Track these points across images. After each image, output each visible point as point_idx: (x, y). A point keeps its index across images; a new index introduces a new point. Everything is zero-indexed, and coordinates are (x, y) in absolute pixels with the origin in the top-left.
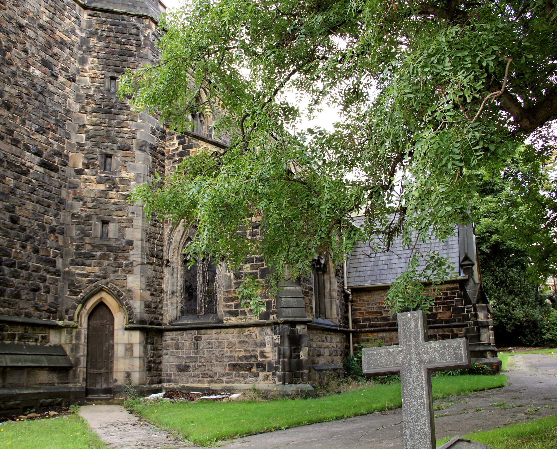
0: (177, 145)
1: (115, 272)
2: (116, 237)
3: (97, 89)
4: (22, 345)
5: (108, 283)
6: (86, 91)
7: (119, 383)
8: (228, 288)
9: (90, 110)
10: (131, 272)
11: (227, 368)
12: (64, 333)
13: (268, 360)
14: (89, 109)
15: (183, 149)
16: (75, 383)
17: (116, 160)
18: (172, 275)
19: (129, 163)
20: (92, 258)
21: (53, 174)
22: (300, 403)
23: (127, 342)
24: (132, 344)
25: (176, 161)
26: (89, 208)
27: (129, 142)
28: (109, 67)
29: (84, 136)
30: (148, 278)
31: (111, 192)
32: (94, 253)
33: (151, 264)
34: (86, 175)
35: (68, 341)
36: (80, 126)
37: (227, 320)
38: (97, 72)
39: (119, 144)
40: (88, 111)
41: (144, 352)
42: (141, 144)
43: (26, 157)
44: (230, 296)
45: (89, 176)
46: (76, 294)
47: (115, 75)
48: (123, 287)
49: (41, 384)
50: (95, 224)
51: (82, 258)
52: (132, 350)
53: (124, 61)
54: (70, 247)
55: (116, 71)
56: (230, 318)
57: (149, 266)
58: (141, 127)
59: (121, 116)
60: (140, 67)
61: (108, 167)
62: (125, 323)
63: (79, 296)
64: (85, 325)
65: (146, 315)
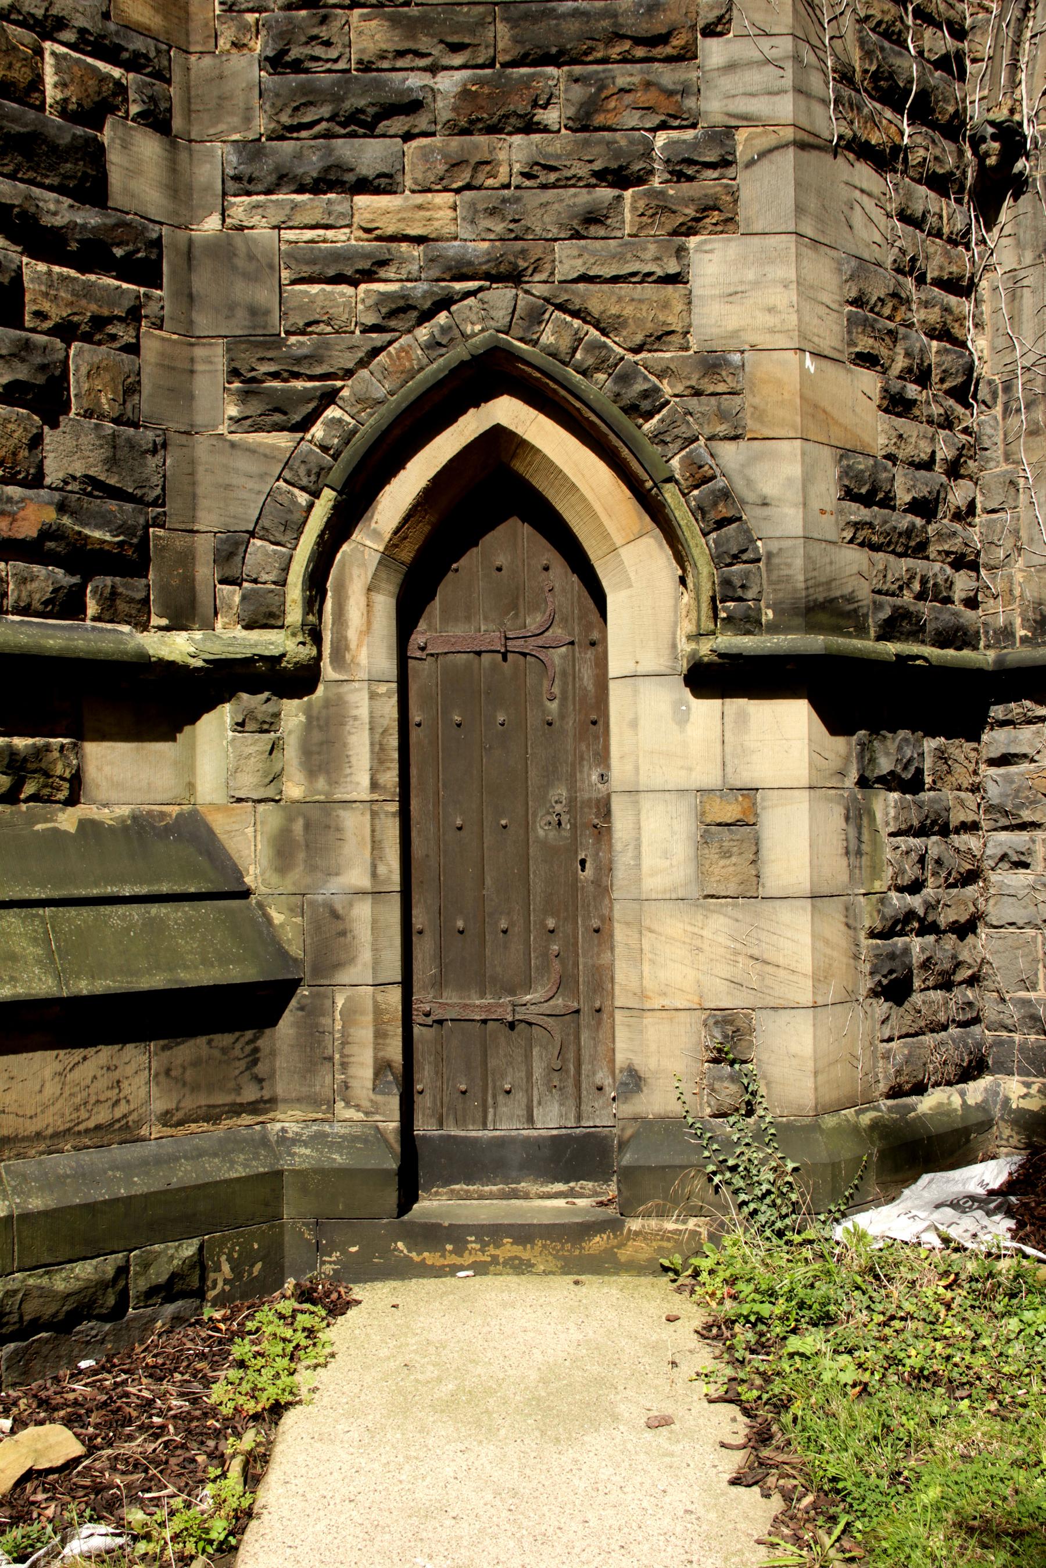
5: (535, 317)
7: (658, 1101)
10: (717, 215)
12: (215, 730)
20: (398, 124)
23: (708, 776)
30: (863, 267)
32: (415, 81)
33: (884, 159)
35: (248, 783)
41: (853, 852)
48: (659, 338)
57: (864, 174)
62: (688, 627)
65: (854, 558)
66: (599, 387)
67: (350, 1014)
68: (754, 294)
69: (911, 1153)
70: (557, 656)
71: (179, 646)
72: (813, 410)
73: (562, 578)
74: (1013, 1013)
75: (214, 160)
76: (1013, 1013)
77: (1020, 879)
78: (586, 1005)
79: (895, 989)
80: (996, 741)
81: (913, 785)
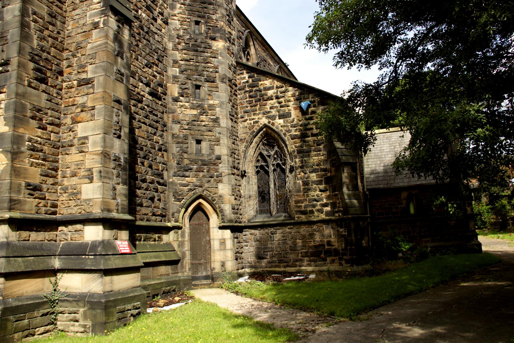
0: (247, 78)
1: (209, 181)
2: (208, 153)
3: (185, 31)
4: (146, 245)
5: (203, 191)
6: (177, 32)
7: (216, 271)
8: (298, 192)
9: (181, 48)
10: (221, 181)
11: (300, 255)
12: (172, 233)
13: (334, 247)
14: (180, 47)
15: (253, 81)
16: (183, 272)
17: (204, 90)
18: (249, 183)
19: (214, 92)
20: (190, 171)
21: (157, 101)
22: (366, 280)
23: (221, 238)
24: (225, 239)
25: (247, 91)
26: (185, 129)
27: (213, 75)
28: (194, 12)
29: (178, 70)
30: (233, 186)
31: (201, 116)
32: (192, 166)
33: (233, 174)
34: (181, 102)
35: (175, 239)
36: (174, 61)
37: (298, 218)
38: (184, 16)
39: (205, 77)
40: (179, 49)
41: (233, 245)
42: (222, 77)
43: (140, 87)
44: (300, 199)
45: (184, 103)
46: (179, 200)
47: (199, 19)
48: (215, 194)
49: (161, 275)
50: (191, 143)
51: (183, 171)
52: (225, 244)
53: (205, 8)
54: (172, 162)
55: (199, 17)
56: (301, 216)
57: (233, 176)
58: (222, 63)
59: (206, 54)
60: (218, 13)
61: (197, 96)
62: (218, 223)
63: (182, 202)
64: (187, 225)
65: (233, 215)
66: (210, 198)
67: (186, 263)
68: (224, 189)
69: (240, 276)
70: (204, 225)
71: (169, 224)
72: (230, 201)
73: (205, 217)
74: (246, 262)
75: (172, 173)
76: (246, 262)
77: (247, 248)
78: (208, 261)
79: (237, 259)
80: (244, 233)
81: (237, 238)
